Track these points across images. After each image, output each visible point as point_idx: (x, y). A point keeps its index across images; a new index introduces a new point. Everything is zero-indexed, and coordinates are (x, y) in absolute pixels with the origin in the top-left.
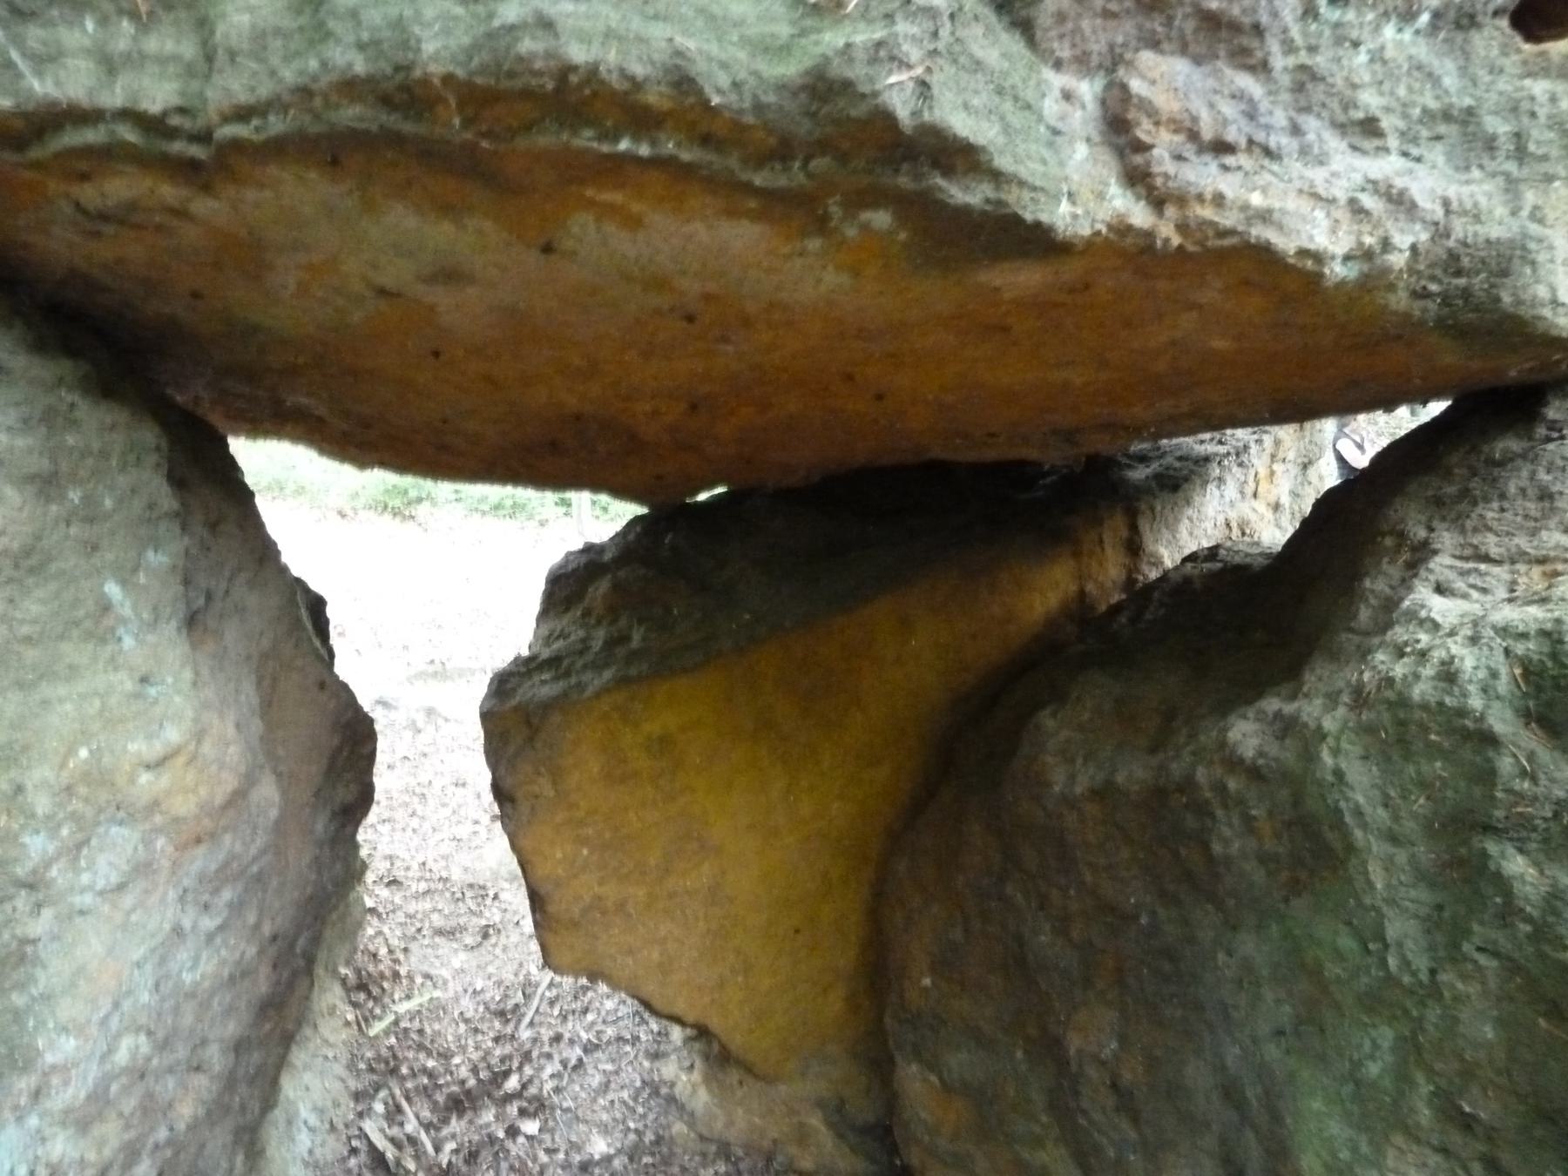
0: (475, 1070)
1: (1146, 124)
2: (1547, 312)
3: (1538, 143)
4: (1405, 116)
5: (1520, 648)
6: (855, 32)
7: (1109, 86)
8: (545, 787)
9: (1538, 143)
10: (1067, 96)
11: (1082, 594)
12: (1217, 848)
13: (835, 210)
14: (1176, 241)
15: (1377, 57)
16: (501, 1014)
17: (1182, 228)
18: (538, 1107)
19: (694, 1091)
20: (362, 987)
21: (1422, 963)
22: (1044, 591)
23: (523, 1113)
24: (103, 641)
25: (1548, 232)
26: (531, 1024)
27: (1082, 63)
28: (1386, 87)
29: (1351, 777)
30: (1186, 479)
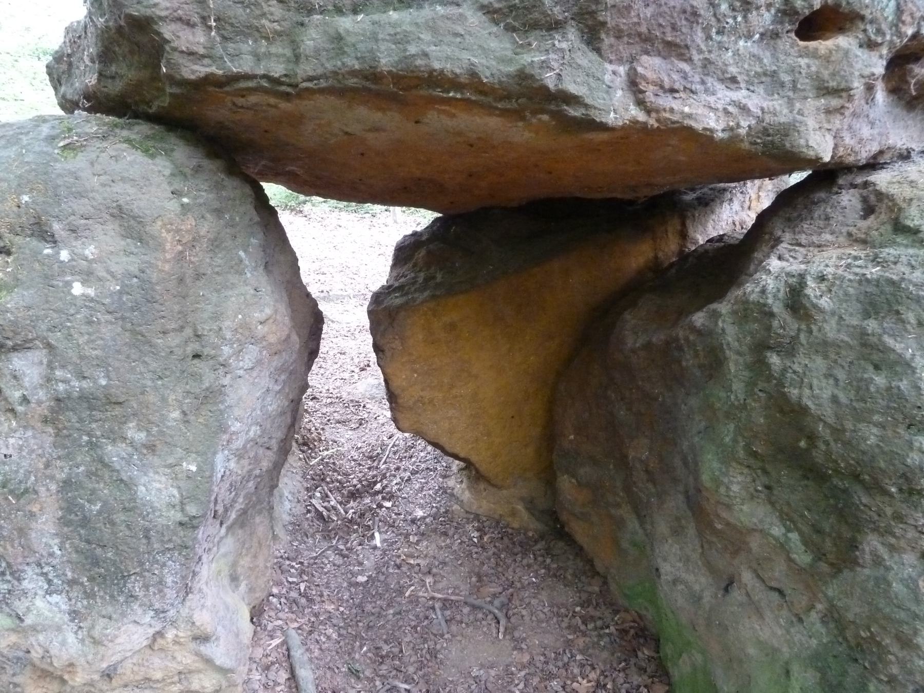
0: (360, 481)
1: (644, 84)
2: (805, 150)
3: (802, 84)
4: (748, 75)
5: (791, 280)
6: (535, 56)
7: (630, 69)
8: (397, 344)
9: (802, 84)
10: (614, 73)
11: (656, 257)
12: (684, 364)
13: (528, 114)
14: (656, 125)
15: (736, 53)
16: (371, 458)
17: (658, 120)
18: (391, 497)
19: (463, 492)
20: (305, 444)
21: (741, 397)
22: (637, 256)
23: (384, 498)
24: (241, 274)
25: (805, 119)
26: (385, 463)
27: (620, 61)
28: (740, 65)
29: (727, 331)
30: (713, 200)
